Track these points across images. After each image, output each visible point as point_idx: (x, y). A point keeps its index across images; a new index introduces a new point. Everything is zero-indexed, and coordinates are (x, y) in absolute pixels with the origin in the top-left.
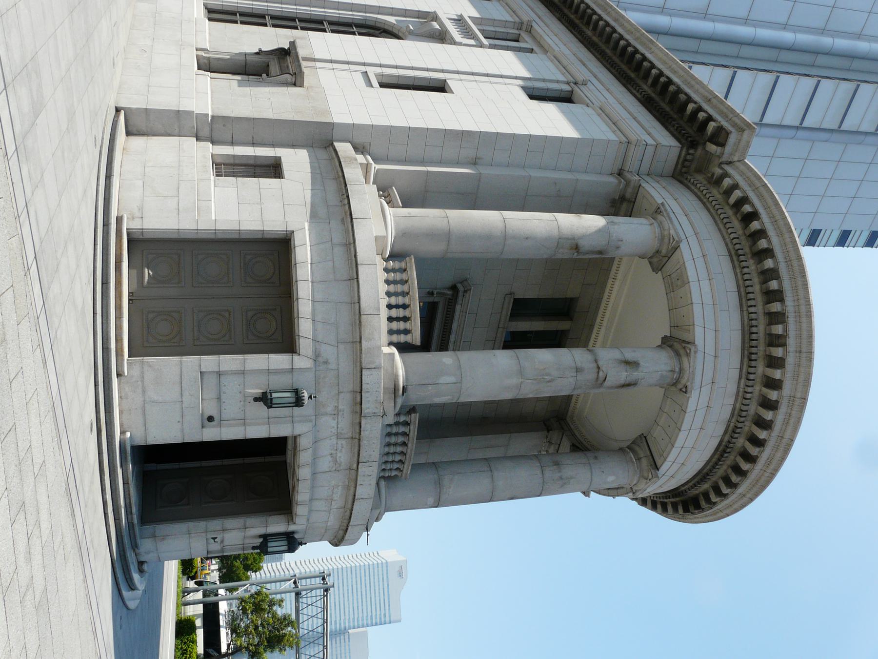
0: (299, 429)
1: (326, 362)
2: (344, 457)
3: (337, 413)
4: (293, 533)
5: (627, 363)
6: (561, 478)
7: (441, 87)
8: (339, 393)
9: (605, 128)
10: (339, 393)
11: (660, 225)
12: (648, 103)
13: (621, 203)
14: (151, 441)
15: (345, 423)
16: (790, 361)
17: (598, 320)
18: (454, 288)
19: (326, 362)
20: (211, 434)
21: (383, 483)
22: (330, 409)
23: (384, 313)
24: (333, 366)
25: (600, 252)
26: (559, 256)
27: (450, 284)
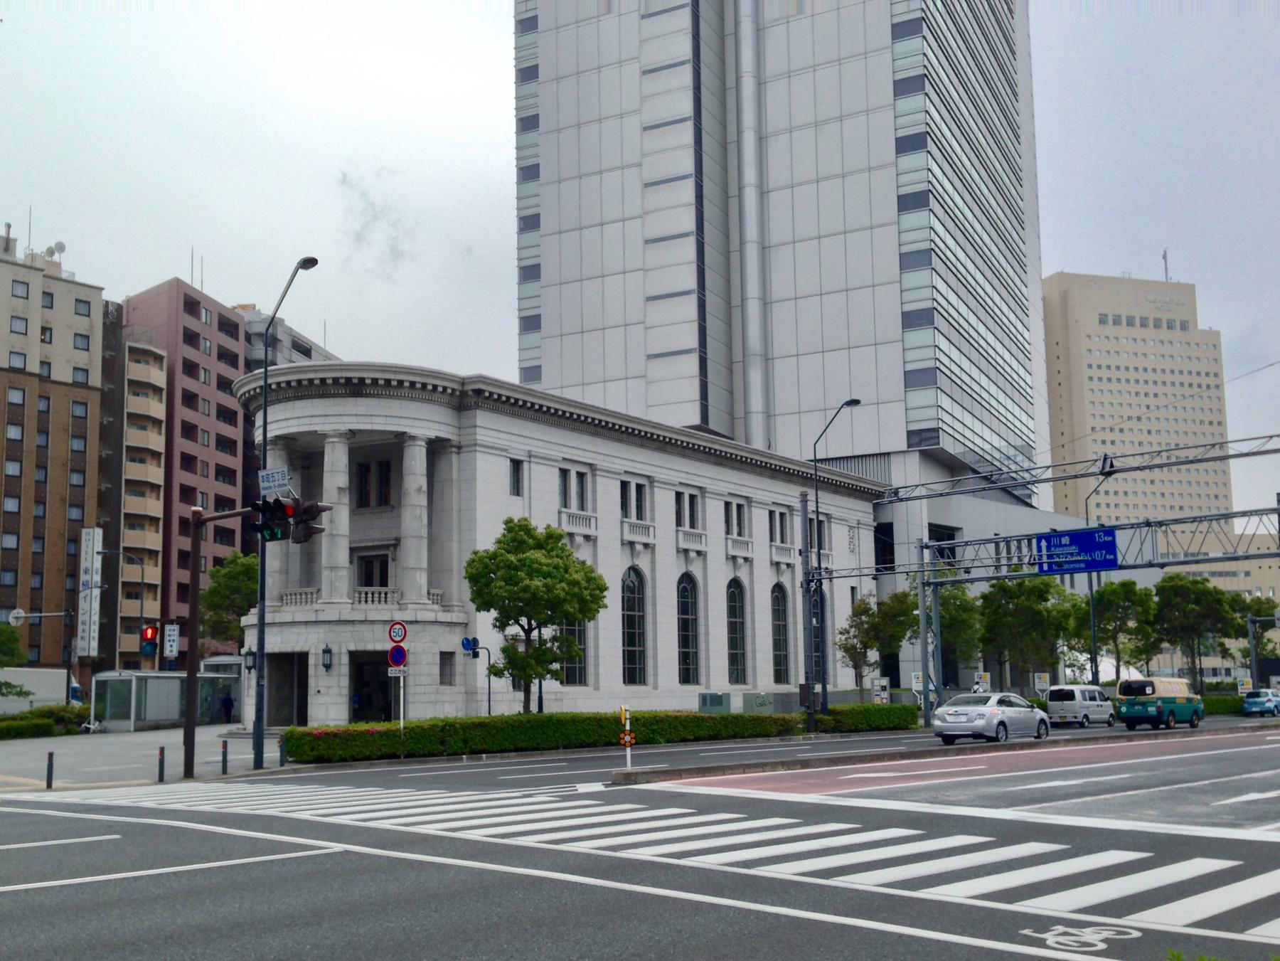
0: (344, 650)
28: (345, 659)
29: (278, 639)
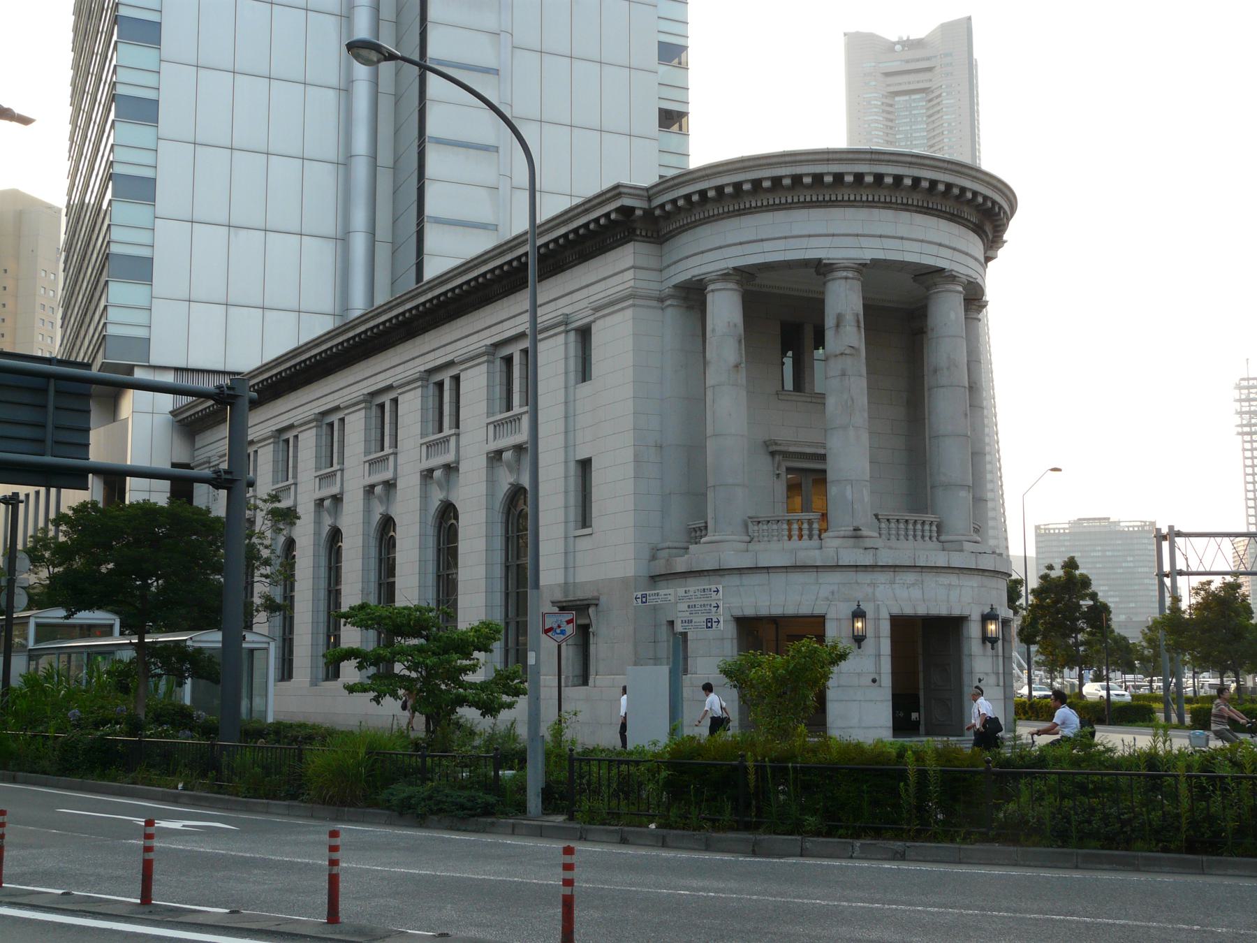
0: (885, 615)
1: (833, 593)
2: (910, 577)
3: (873, 585)
4: (1044, 578)
5: (838, 326)
6: (948, 368)
7: (585, 465)
8: (857, 583)
9: (618, 318)
10: (857, 583)
11: (713, 281)
12: (585, 257)
13: (693, 296)
14: (891, 724)
15: (881, 577)
16: (836, 168)
17: (805, 295)
18: (773, 454)
19: (833, 593)
20: (886, 680)
21: (943, 538)
22: (870, 590)
23: (795, 544)
24: (835, 588)
25: (740, 341)
26: (744, 382)
27: (769, 458)
28: (886, 627)
29: (916, 593)
